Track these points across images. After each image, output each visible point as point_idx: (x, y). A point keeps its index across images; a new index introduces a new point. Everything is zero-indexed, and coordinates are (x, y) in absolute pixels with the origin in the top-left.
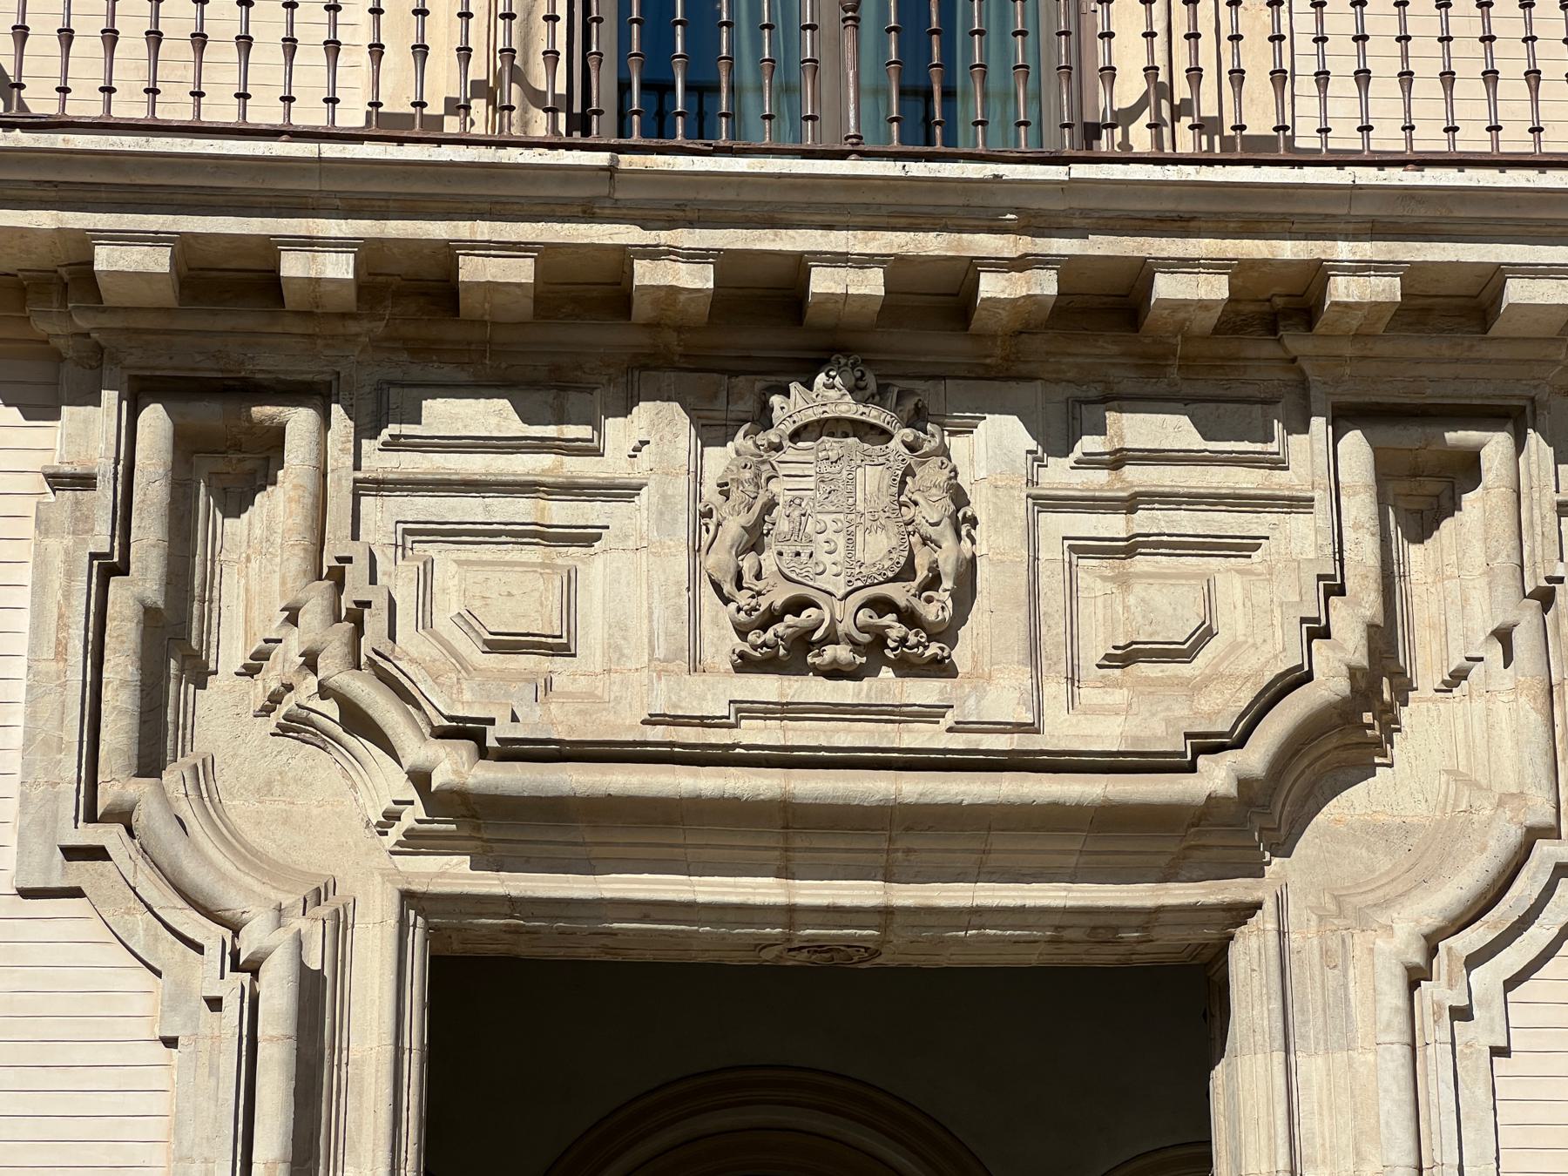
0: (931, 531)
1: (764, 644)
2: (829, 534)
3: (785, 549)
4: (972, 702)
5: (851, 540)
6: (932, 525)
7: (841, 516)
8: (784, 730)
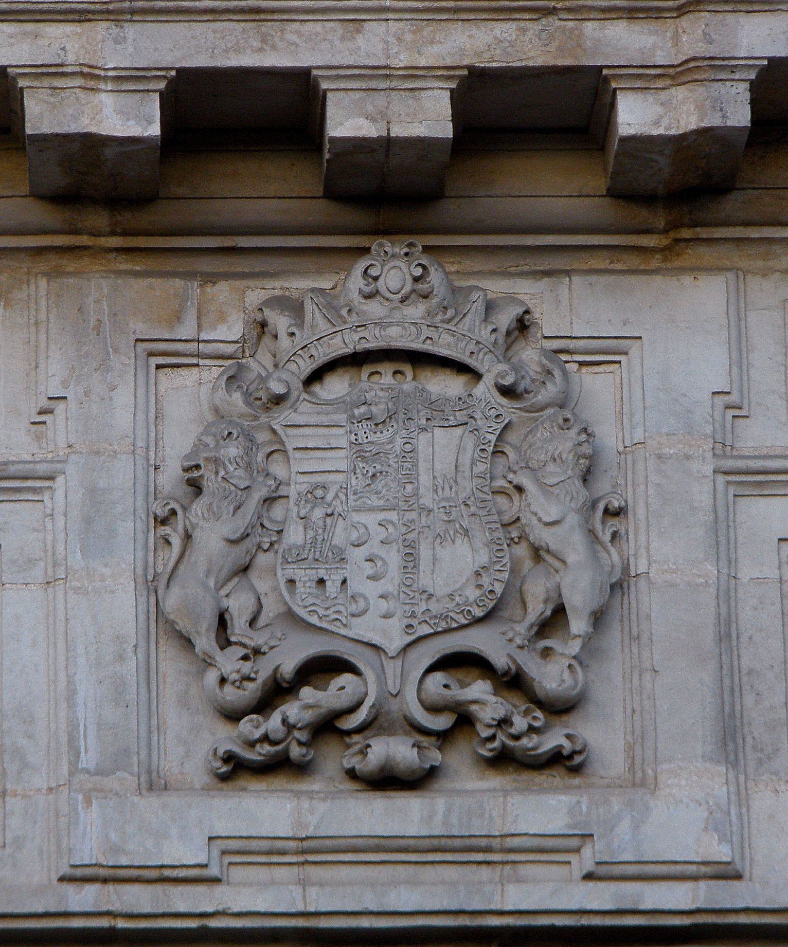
0: (545, 536)
1: (265, 738)
2: (374, 547)
3: (299, 574)
4: (624, 827)
5: (410, 557)
6: (547, 524)
7: (393, 516)
8: (304, 883)
